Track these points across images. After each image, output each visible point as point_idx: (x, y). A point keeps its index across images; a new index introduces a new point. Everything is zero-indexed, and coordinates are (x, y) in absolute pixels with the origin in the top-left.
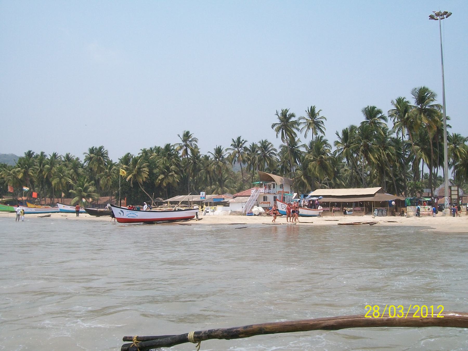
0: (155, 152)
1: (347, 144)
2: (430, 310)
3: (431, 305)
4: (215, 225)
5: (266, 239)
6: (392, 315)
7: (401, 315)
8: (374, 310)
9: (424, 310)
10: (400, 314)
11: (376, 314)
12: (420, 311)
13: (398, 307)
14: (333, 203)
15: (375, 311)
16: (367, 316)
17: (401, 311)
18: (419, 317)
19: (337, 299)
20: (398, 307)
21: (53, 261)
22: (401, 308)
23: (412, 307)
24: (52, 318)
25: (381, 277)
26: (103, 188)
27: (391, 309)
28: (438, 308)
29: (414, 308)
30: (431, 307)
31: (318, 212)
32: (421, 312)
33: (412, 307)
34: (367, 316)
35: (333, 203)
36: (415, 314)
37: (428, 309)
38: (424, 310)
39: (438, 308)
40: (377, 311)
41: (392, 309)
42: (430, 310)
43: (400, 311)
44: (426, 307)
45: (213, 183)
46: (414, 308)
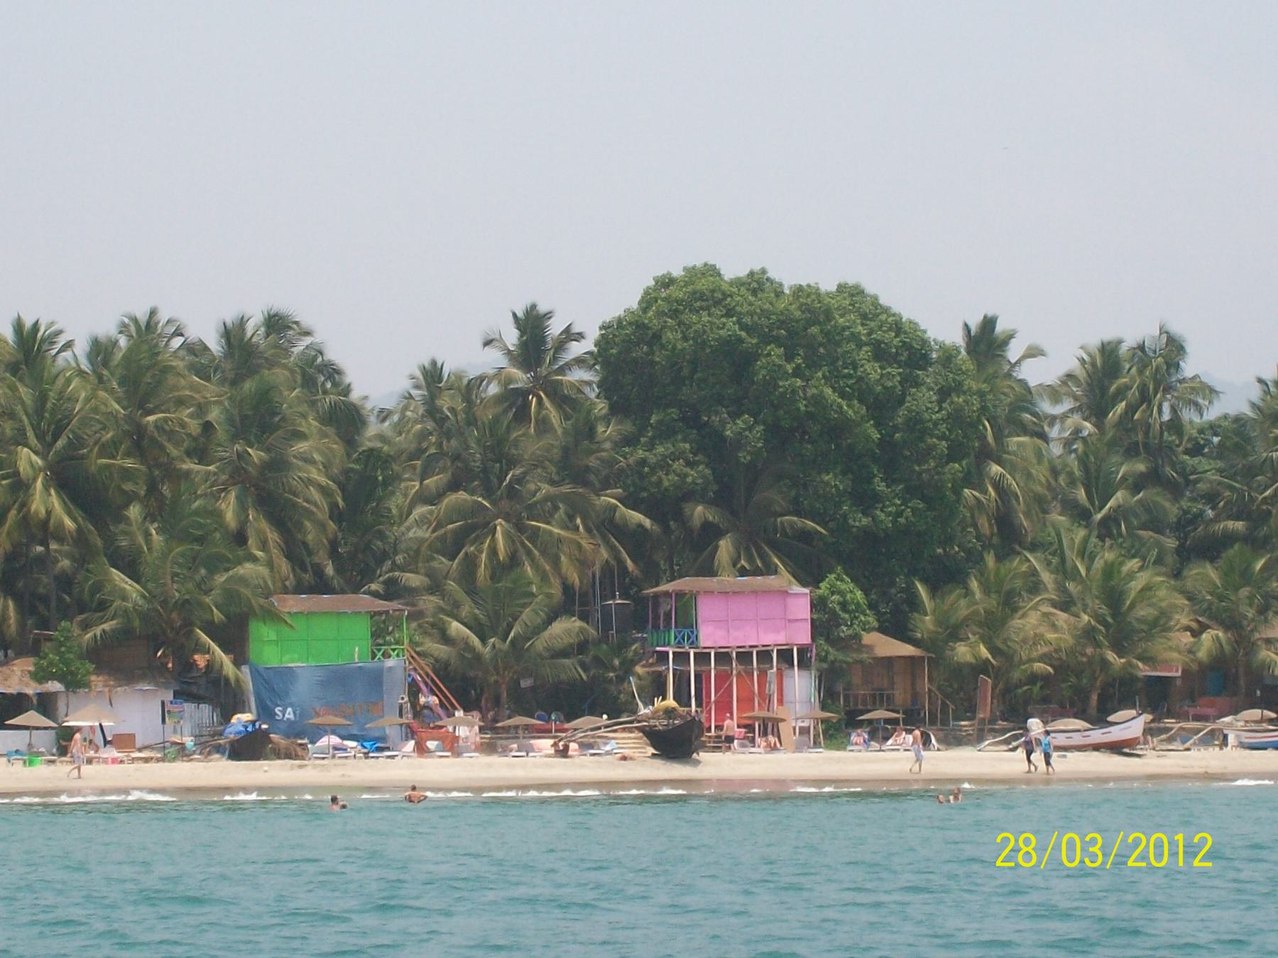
0: (875, 593)
2: (1173, 843)
3: (1177, 834)
4: (189, 790)
8: (1021, 844)
9: (1159, 845)
10: (1093, 857)
13: (1087, 839)
14: (677, 679)
15: (1025, 849)
16: (1136, 860)
18: (1144, 864)
20: (1087, 839)
22: (1094, 841)
24: (316, 860)
30: (1176, 838)
31: (799, 675)
32: (1148, 852)
34: (1136, 860)
35: (677, 679)
36: (1001, 858)
37: (1169, 843)
38: (1159, 845)
39: (999, 840)
41: (1071, 844)
42: (1173, 843)
43: (1091, 849)
44: (1076, 837)
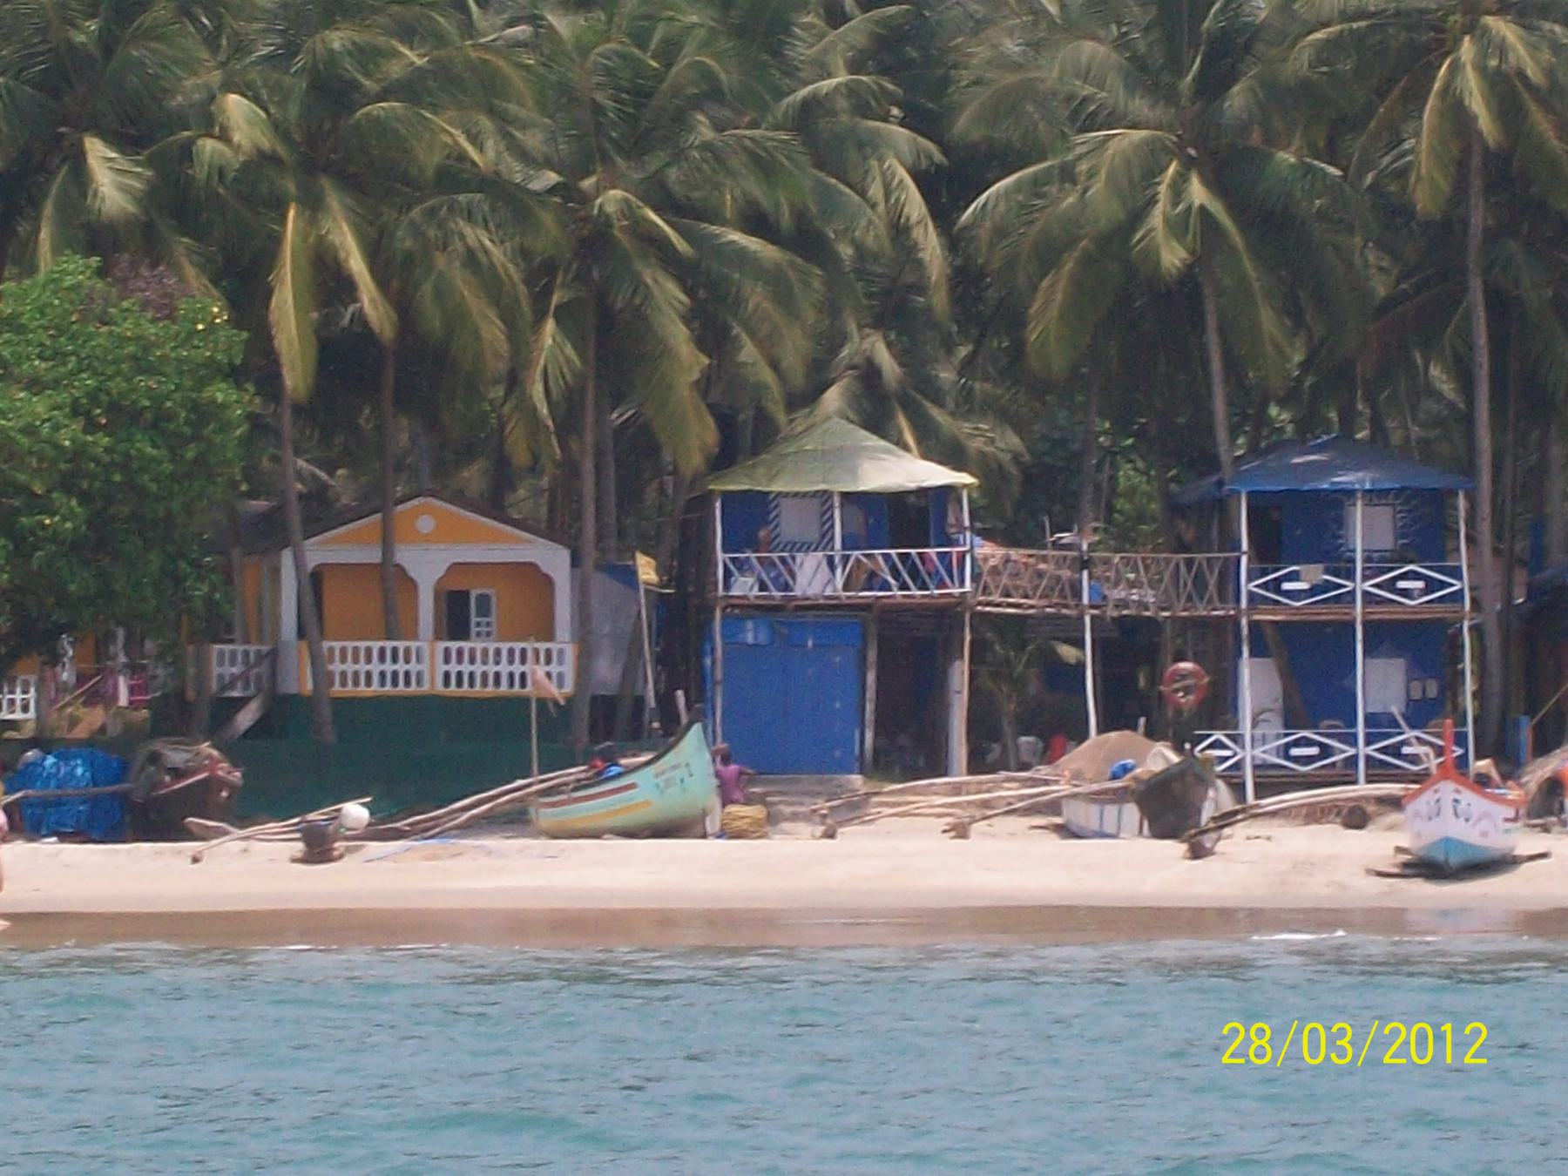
1: (315, 232)
5: (1282, 776)
6: (1314, 1055)
7: (1342, 1056)
8: (1253, 1037)
11: (1260, 1054)
12: (1407, 1043)
16: (1233, 1055)
17: (1344, 1042)
18: (1404, 1061)
19: (939, 986)
21: (853, 947)
23: (1381, 1028)
25: (1340, 933)
26: (281, 150)
27: (1426, 1049)
28: (1467, 1031)
29: (1387, 1031)
30: (1443, 1029)
33: (1381, 1028)
34: (1233, 1055)
39: (1467, 1031)
40: (1264, 1042)
43: (1338, 1043)
45: (1112, 353)
46: (1387, 1031)
